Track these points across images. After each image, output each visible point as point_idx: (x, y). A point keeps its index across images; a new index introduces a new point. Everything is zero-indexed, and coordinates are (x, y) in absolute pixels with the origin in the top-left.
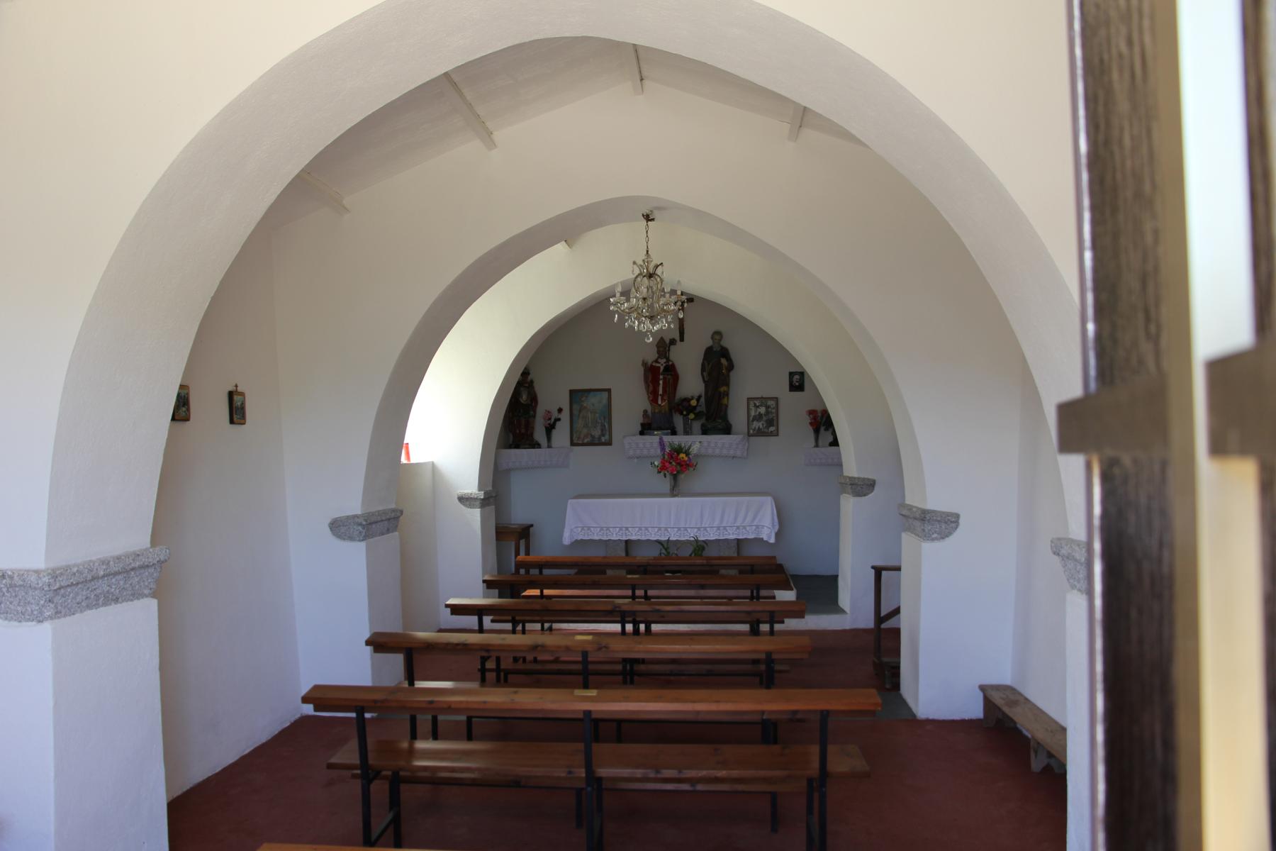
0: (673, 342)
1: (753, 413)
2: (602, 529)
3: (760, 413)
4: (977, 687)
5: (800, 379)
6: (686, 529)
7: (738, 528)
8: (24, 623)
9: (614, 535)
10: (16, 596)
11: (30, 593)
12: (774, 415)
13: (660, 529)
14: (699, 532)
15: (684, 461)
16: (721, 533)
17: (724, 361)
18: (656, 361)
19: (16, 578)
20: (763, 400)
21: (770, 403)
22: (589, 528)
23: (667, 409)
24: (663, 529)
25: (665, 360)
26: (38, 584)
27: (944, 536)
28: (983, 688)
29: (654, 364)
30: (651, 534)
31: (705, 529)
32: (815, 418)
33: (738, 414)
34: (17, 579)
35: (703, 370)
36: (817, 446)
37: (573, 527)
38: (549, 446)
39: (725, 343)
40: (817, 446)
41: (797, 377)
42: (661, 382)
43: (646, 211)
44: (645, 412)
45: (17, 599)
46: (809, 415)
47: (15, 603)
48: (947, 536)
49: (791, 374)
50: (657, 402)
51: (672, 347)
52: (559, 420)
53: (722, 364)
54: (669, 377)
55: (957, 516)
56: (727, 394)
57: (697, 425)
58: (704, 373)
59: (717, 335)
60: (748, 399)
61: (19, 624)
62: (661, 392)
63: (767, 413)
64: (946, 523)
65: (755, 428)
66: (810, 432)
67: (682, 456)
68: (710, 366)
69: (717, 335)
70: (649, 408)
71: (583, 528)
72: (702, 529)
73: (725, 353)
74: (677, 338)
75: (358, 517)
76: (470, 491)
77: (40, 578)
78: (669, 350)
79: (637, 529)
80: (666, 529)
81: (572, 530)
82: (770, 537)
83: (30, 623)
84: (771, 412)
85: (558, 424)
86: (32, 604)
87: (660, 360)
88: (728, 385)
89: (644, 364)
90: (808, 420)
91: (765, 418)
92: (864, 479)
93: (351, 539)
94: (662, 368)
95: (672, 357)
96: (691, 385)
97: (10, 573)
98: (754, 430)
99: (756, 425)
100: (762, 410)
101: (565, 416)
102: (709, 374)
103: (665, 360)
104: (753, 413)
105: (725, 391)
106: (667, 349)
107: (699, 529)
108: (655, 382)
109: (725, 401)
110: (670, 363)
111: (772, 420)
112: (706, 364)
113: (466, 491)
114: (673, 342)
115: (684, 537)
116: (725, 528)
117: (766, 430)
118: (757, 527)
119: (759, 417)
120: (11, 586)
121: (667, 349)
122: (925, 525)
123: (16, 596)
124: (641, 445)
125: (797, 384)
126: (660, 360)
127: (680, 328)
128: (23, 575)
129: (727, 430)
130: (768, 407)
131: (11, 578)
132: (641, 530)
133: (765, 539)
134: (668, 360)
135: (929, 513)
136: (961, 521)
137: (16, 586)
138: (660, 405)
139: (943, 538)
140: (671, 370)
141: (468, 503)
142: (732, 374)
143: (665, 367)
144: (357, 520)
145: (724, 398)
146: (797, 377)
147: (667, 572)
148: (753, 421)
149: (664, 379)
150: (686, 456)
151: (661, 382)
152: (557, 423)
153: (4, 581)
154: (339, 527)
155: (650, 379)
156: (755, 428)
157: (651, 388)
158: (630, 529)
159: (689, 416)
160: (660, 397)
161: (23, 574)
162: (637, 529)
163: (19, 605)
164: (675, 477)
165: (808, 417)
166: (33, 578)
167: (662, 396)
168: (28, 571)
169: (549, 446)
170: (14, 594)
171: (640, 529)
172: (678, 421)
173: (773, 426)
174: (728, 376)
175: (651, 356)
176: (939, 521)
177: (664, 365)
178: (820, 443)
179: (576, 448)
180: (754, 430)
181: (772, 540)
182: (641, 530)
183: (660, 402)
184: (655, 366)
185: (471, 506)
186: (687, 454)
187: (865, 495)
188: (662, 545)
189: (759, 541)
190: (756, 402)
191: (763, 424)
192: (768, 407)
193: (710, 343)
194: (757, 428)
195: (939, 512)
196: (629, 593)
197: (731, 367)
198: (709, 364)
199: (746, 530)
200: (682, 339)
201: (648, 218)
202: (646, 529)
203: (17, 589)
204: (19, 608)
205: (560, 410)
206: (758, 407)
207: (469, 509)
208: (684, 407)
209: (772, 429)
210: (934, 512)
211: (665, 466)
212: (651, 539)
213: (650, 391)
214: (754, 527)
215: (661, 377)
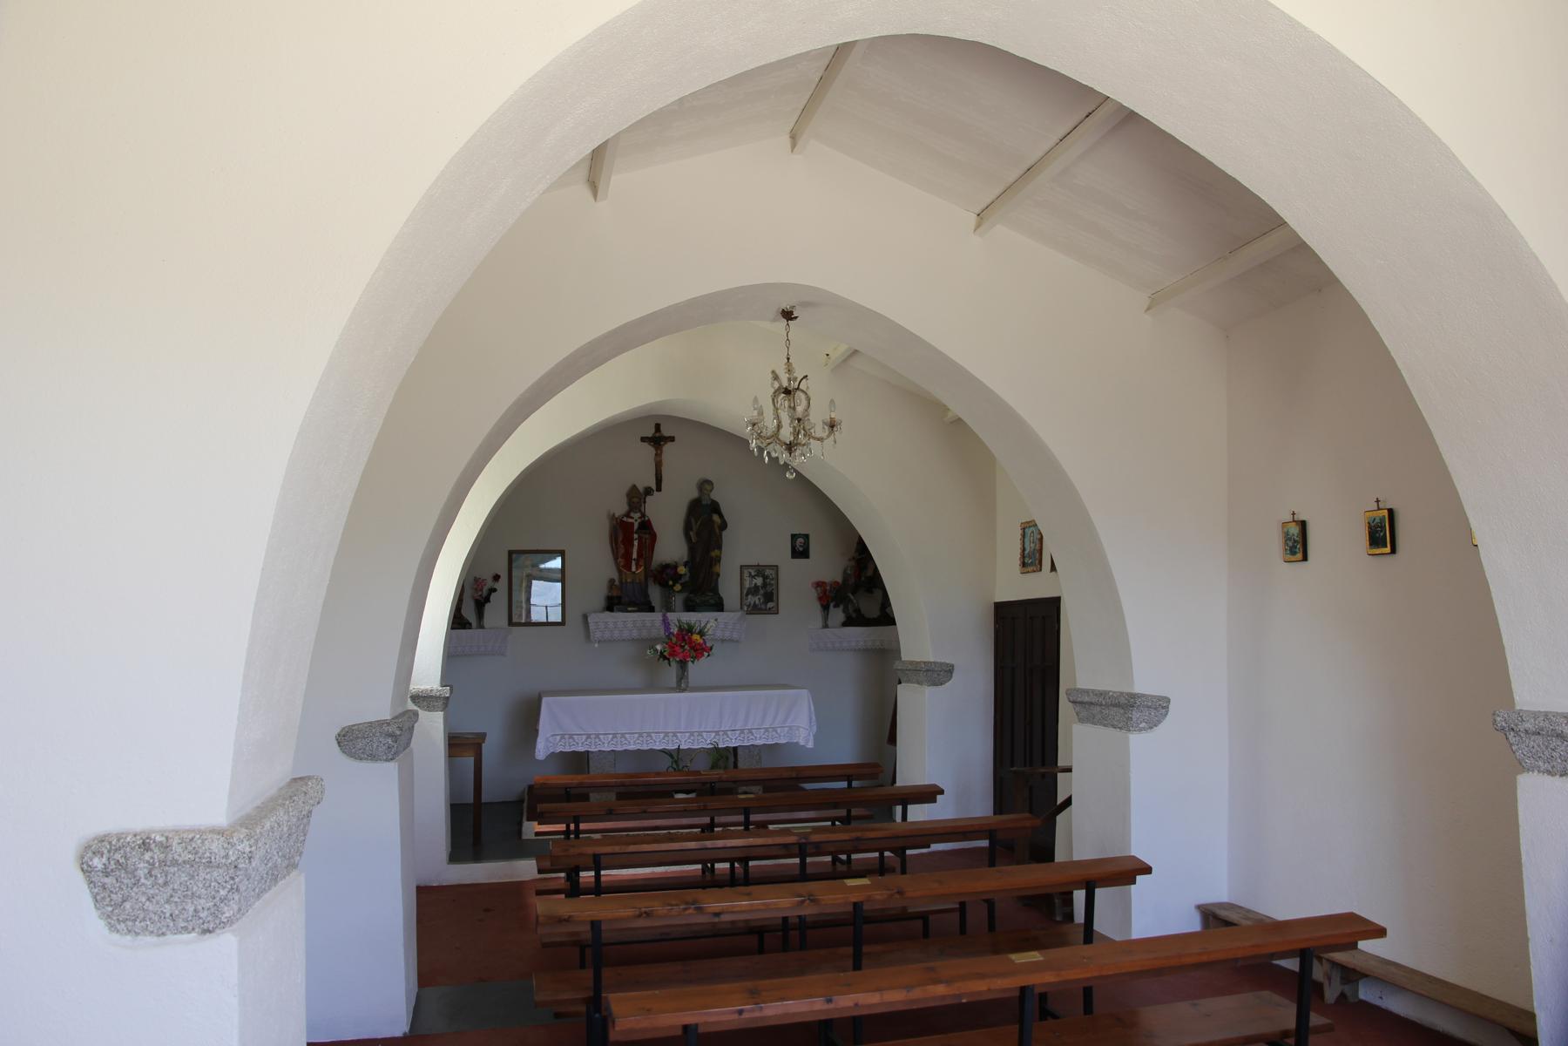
0: (648, 491)
1: (747, 585)
2: (589, 736)
3: (756, 584)
4: (1193, 908)
5: (804, 544)
6: (700, 733)
7: (767, 730)
8: (170, 937)
9: (733, 741)
10: (166, 884)
11: (202, 875)
12: (774, 587)
13: (666, 734)
14: (717, 737)
15: (699, 644)
16: (619, 742)
17: (716, 518)
18: (628, 515)
19: (176, 847)
20: (760, 570)
21: (768, 572)
22: (571, 736)
23: (642, 578)
24: (696, 734)
25: (638, 515)
26: (227, 856)
27: (1152, 725)
28: (1199, 907)
29: (625, 519)
30: (655, 742)
31: (725, 732)
32: (825, 592)
33: (729, 587)
34: (179, 850)
35: (687, 528)
36: (826, 626)
37: (548, 735)
38: (481, 626)
39: (715, 496)
40: (826, 626)
41: (800, 540)
42: (636, 543)
43: (786, 306)
44: (612, 581)
45: (169, 890)
46: (816, 588)
47: (161, 898)
48: (1156, 726)
49: (794, 537)
50: (629, 568)
51: (649, 499)
52: (495, 590)
53: (713, 522)
54: (647, 536)
55: (1168, 701)
56: (718, 560)
57: (678, 600)
58: (691, 533)
59: (705, 485)
60: (741, 566)
61: (161, 938)
62: (635, 556)
63: (765, 585)
64: (1155, 709)
65: (750, 604)
66: (817, 607)
67: (696, 637)
68: (699, 523)
69: (705, 485)
70: (615, 576)
71: (563, 736)
72: (721, 733)
73: (715, 508)
74: (654, 487)
75: (388, 724)
76: (428, 687)
77: (233, 845)
78: (645, 502)
79: (636, 735)
80: (675, 734)
81: (547, 739)
82: (807, 741)
83: (185, 937)
84: (770, 584)
85: (493, 595)
86: (200, 897)
87: (632, 514)
88: (720, 548)
89: (612, 517)
90: (813, 594)
91: (762, 592)
92: (941, 664)
93: (373, 757)
94: (636, 526)
95: (648, 513)
96: (671, 547)
97: (158, 838)
98: (749, 606)
99: (752, 599)
100: (759, 581)
101: (502, 585)
102: (698, 534)
103: (638, 515)
104: (747, 585)
105: (717, 556)
106: (643, 500)
107: (717, 733)
108: (628, 542)
109: (716, 569)
110: (647, 519)
111: (772, 593)
112: (693, 520)
113: (422, 687)
114: (648, 491)
115: (698, 744)
116: (750, 731)
117: (763, 607)
118: (790, 728)
119: (754, 590)
120: (163, 863)
121: (643, 500)
122: (1134, 713)
123: (166, 884)
124: (611, 625)
125: (801, 549)
126: (632, 514)
127: (656, 474)
128: (192, 840)
129: (719, 606)
130: (765, 578)
131: (165, 847)
132: (616, 737)
133: (802, 743)
134: (643, 515)
135: (1139, 697)
136: (1171, 707)
137: (175, 863)
138: (634, 572)
139: (1151, 728)
140: (646, 526)
141: (425, 703)
142: (724, 533)
143: (639, 523)
144: (386, 728)
145: (715, 564)
146: (800, 540)
147: (677, 792)
148: (747, 595)
149: (640, 539)
150: (701, 637)
151: (636, 543)
152: (493, 594)
153: (147, 856)
154: (1157, 708)
155: (620, 539)
156: (750, 604)
157: (622, 551)
158: (627, 736)
159: (675, 588)
160: (633, 563)
161: (190, 838)
162: (636, 735)
163: (168, 902)
164: (683, 665)
165: (813, 590)
166: (216, 846)
167: (637, 561)
168: (201, 832)
169: (481, 626)
170: (161, 881)
171: (641, 735)
172: (655, 594)
173: (772, 601)
174: (721, 536)
175: (620, 508)
176: (1149, 707)
177: (639, 521)
178: (830, 623)
179: (515, 629)
180: (749, 606)
181: (810, 745)
182: (616, 737)
183: (634, 569)
184: (626, 523)
185: (429, 709)
186: (701, 633)
187: (941, 684)
188: (671, 756)
189: (792, 746)
190: (750, 570)
191: (759, 599)
192: (765, 578)
193: (695, 494)
194: (752, 603)
195: (1150, 696)
196: (741, 818)
197: (724, 526)
198: (697, 522)
199: (777, 732)
200: (659, 489)
201: (788, 315)
202: (649, 734)
203: (172, 870)
204: (168, 909)
205: (497, 578)
206: (753, 577)
207: (426, 712)
208: (665, 575)
209: (770, 605)
210: (1143, 695)
211: (674, 651)
212: (654, 748)
213: (620, 554)
214: (786, 729)
215: (636, 536)
